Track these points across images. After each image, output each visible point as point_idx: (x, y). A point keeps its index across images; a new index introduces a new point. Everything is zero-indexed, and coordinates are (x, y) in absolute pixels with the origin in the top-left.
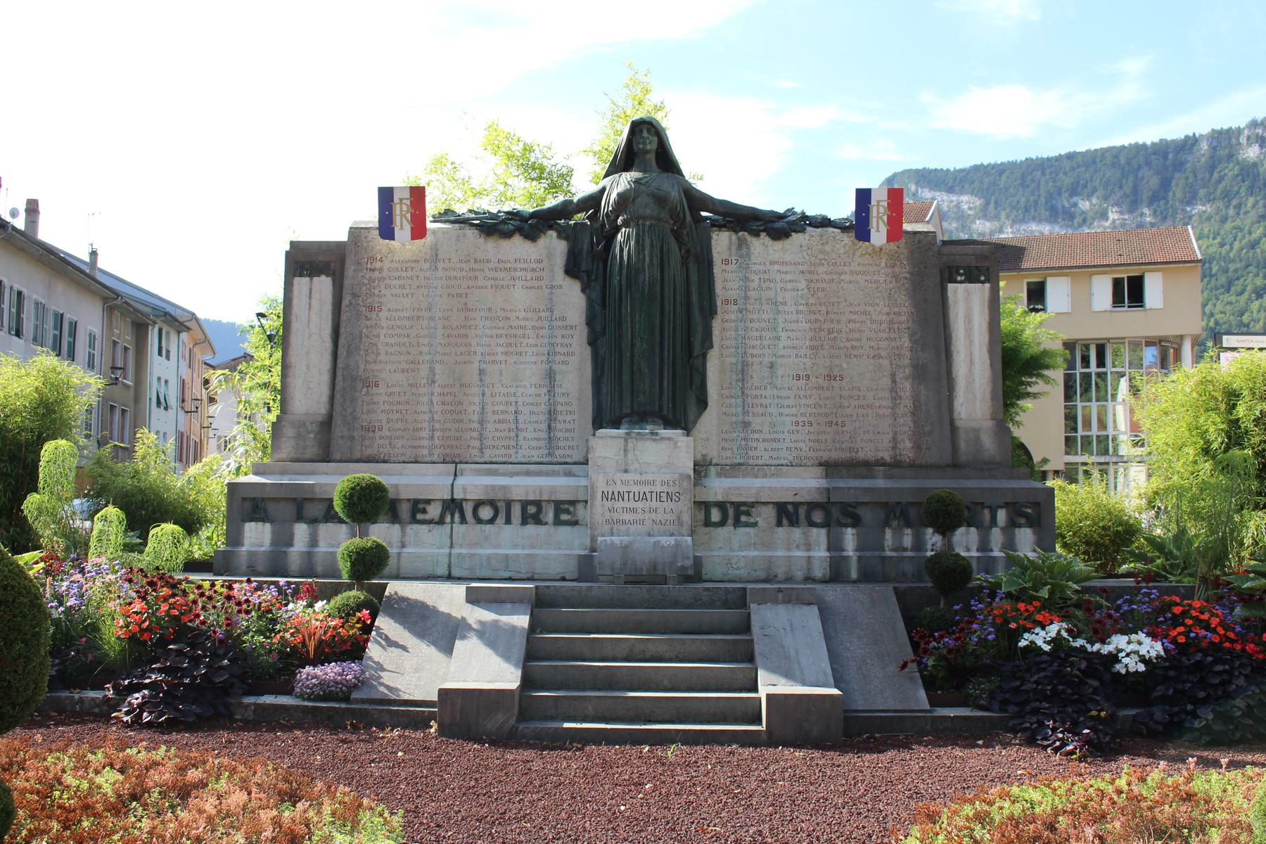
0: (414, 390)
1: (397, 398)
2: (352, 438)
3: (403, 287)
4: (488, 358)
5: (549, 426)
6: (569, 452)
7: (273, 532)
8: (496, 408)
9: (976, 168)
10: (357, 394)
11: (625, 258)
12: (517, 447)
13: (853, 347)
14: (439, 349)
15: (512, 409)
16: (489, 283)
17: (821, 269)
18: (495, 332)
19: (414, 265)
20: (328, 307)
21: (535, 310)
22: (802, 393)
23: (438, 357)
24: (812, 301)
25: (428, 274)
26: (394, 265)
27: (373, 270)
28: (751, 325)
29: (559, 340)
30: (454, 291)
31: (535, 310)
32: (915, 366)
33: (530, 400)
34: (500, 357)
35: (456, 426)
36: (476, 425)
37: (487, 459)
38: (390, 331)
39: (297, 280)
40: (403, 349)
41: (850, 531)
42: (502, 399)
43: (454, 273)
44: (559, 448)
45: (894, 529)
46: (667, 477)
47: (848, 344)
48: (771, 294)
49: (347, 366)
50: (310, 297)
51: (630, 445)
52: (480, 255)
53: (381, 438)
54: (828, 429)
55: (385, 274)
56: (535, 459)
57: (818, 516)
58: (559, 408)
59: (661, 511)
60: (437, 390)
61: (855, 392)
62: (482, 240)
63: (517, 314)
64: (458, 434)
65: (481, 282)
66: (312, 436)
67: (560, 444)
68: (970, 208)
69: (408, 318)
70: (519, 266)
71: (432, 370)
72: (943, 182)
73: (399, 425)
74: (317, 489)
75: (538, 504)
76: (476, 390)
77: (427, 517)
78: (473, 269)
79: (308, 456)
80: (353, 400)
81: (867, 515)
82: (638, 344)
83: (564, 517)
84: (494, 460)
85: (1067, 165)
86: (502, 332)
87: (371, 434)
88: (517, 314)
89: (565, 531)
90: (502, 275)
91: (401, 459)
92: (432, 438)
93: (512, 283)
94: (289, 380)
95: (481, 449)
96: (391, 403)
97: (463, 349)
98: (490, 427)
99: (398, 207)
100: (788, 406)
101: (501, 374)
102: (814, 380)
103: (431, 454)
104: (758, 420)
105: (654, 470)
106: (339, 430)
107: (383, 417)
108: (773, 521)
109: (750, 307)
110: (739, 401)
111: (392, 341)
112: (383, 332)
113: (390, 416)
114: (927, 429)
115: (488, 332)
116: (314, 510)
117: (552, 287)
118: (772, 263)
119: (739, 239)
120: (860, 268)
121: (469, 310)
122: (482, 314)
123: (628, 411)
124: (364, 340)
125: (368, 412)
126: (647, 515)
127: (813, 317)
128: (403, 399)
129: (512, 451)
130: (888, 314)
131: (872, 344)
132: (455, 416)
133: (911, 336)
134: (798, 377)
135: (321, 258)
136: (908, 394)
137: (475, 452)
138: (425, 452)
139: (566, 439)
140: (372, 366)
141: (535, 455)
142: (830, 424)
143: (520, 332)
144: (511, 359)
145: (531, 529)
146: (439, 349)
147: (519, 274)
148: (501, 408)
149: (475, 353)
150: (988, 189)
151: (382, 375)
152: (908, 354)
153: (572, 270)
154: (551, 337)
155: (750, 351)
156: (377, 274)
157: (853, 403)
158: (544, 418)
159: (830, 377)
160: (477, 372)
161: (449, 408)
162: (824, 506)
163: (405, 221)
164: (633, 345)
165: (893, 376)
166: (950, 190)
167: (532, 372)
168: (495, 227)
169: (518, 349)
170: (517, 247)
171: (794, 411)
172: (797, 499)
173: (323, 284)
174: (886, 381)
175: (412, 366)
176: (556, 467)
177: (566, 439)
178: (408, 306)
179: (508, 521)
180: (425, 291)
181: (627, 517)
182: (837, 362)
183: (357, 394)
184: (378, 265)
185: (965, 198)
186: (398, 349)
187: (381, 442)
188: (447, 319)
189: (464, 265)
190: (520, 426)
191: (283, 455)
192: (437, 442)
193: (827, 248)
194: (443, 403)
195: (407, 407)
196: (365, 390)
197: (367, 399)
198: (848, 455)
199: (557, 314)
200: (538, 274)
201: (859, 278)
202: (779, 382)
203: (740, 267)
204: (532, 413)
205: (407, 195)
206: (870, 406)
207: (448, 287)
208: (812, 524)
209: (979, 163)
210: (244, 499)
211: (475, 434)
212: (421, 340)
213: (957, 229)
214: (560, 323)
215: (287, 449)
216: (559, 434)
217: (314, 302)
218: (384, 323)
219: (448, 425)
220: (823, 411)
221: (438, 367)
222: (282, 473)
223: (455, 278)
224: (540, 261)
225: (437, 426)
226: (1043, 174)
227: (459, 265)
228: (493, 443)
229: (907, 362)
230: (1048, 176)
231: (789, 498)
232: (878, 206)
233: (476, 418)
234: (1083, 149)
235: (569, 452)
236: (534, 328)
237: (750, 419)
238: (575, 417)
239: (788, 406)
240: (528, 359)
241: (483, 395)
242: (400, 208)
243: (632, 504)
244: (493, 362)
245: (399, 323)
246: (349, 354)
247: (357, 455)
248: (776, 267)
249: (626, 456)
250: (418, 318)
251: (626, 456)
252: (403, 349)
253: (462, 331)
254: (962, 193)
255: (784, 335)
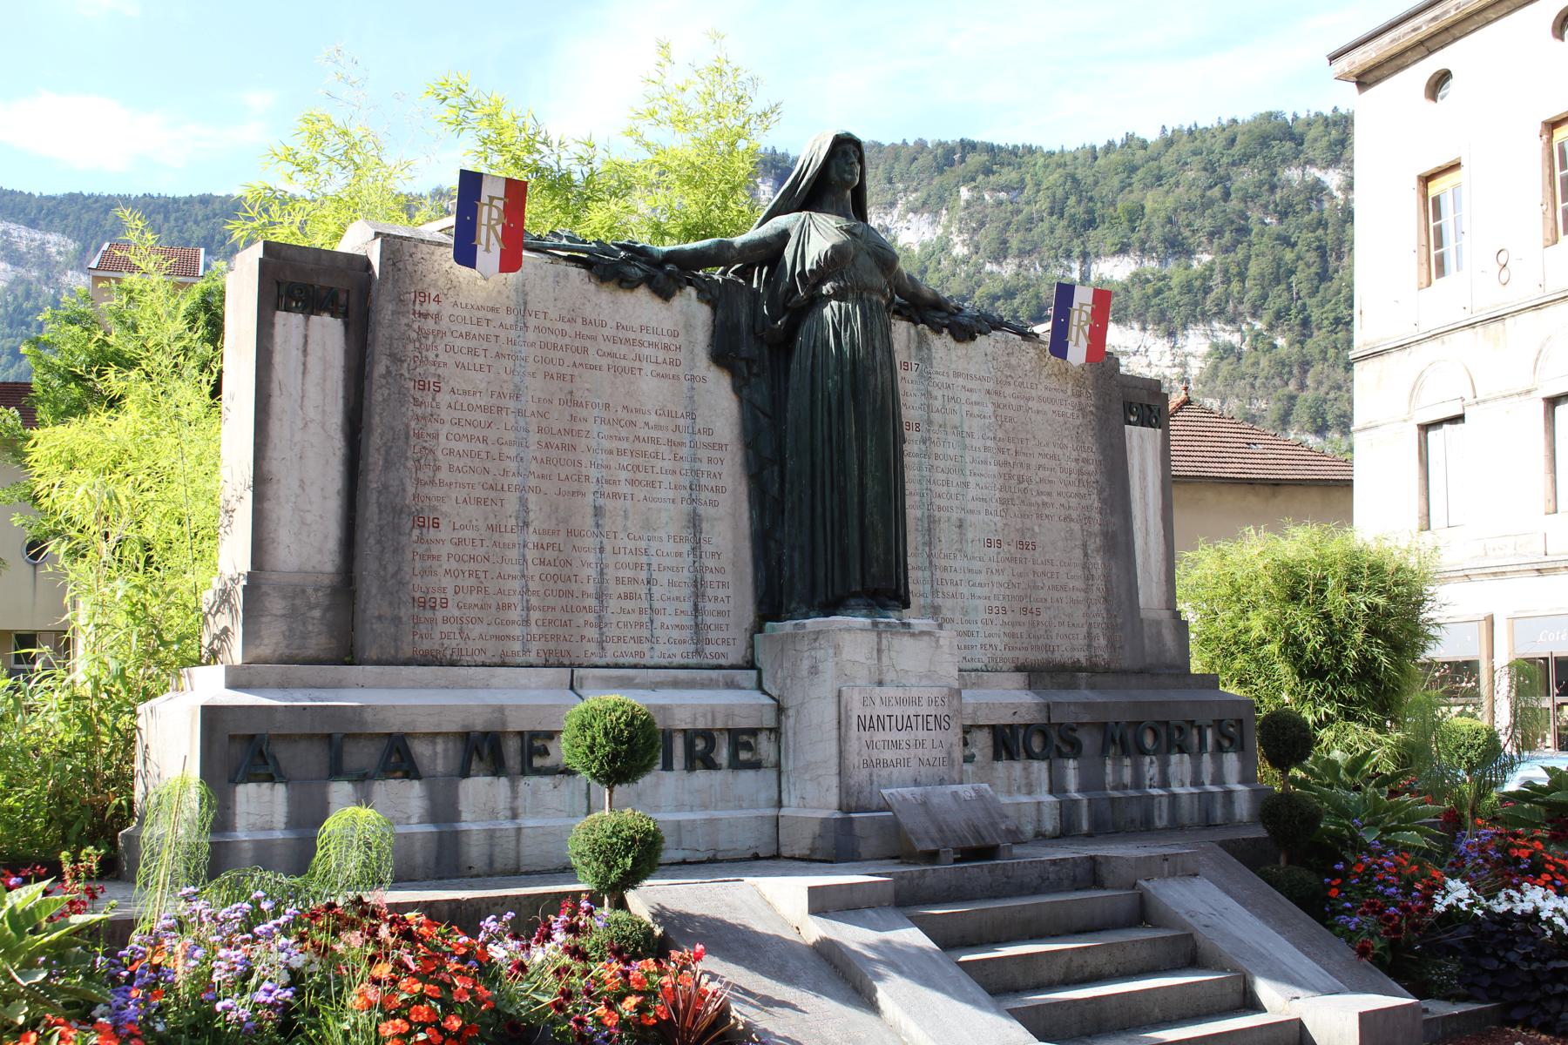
0: (496, 536)
1: (469, 550)
2: (397, 620)
3: (472, 352)
4: (607, 489)
5: (696, 605)
6: (722, 649)
7: (292, 801)
8: (621, 574)
9: (72, 198)
10: (404, 539)
11: (847, 349)
12: (652, 639)
13: (1044, 504)
14: (534, 467)
15: (643, 575)
16: (604, 362)
17: (1008, 390)
18: (616, 444)
19: (490, 316)
20: (337, 375)
21: (670, 414)
22: (994, 566)
23: (533, 482)
24: (1000, 435)
25: (513, 334)
26: (458, 312)
27: (425, 316)
28: (936, 463)
29: (704, 467)
30: (553, 370)
31: (670, 414)
32: (1105, 534)
33: (668, 562)
34: (624, 488)
35: (563, 602)
36: (591, 602)
37: (609, 659)
38: (456, 430)
39: (280, 316)
40: (477, 463)
41: (1071, 764)
42: (629, 559)
43: (552, 339)
44: (709, 642)
45: (1114, 759)
46: (935, 693)
47: (1039, 499)
48: (955, 419)
49: (386, 487)
50: (305, 352)
51: (884, 642)
52: (589, 312)
53: (446, 620)
54: (1023, 619)
55: (444, 324)
56: (678, 660)
57: (1036, 744)
58: (708, 577)
59: (928, 744)
60: (533, 538)
61: (1048, 568)
62: (592, 287)
63: (647, 418)
64: (566, 617)
65: (593, 359)
66: (317, 613)
67: (712, 635)
68: (60, 253)
69: (484, 409)
70: (647, 338)
71: (523, 503)
72: (23, 210)
73: (473, 599)
74: (369, 717)
75: (708, 735)
76: (590, 542)
77: (548, 762)
78: (579, 335)
79: (310, 652)
80: (398, 550)
81: (1088, 740)
82: (870, 484)
83: (744, 755)
84: (621, 661)
85: (200, 212)
86: (625, 445)
87: (429, 614)
88: (647, 418)
89: (747, 776)
90: (623, 349)
91: (479, 659)
92: (526, 622)
93: (637, 364)
94: (267, 505)
95: (601, 644)
96: (460, 559)
97: (570, 470)
98: (613, 604)
99: (486, 209)
100: (980, 585)
101: (626, 517)
102: (1005, 547)
103: (526, 651)
104: (949, 603)
105: (913, 681)
106: (373, 603)
107: (447, 582)
108: (989, 752)
109: (934, 437)
110: (927, 574)
111: (461, 446)
112: (444, 430)
113: (460, 582)
114: (1119, 621)
115: (606, 444)
116: (360, 756)
117: (693, 378)
118: (957, 375)
119: (918, 334)
120: (1047, 394)
121: (577, 404)
122: (596, 412)
123: (859, 589)
124: (413, 441)
125: (424, 573)
126: (913, 751)
127: (1002, 458)
128: (481, 551)
129: (645, 646)
130: (1077, 460)
131: (1063, 501)
132: (560, 585)
133: (1100, 492)
134: (989, 543)
135: (323, 281)
136: (1100, 572)
137: (592, 647)
138: (517, 646)
139: (719, 627)
140: (427, 490)
141: (679, 653)
142: (1025, 610)
143: (651, 448)
144: (640, 492)
145: (701, 777)
146: (534, 467)
147: (647, 351)
148: (629, 573)
149: (587, 478)
150: (87, 230)
151: (445, 508)
152: (1097, 516)
153: (722, 354)
154: (694, 459)
155: (937, 502)
156: (430, 324)
157: (1048, 583)
158: (687, 591)
159: (1022, 545)
160: (590, 511)
161: (551, 570)
162: (1043, 730)
163: (493, 239)
164: (862, 485)
165: (1085, 546)
166: (32, 224)
167: (669, 515)
168: (617, 267)
169: (650, 477)
170: (640, 306)
171: (985, 591)
172: (1017, 720)
173: (328, 331)
174: (1078, 553)
175: (492, 494)
176: (714, 674)
177: (719, 627)
178: (483, 386)
179: (668, 766)
180: (509, 364)
181: (889, 755)
182: (1028, 523)
183: (404, 539)
184: (432, 307)
185: (53, 238)
186: (468, 461)
187: (446, 628)
188: (543, 415)
189: (566, 326)
190: (657, 605)
191: (265, 650)
192: (534, 630)
193: (1013, 361)
194: (542, 562)
195: (486, 566)
196: (416, 532)
197: (421, 549)
198: (1044, 656)
199: (700, 424)
200: (672, 355)
201: (1047, 407)
202: (969, 549)
203: (921, 375)
204: (671, 583)
205: (500, 191)
206: (1064, 588)
207: (544, 360)
208: (1031, 756)
209: (76, 191)
210: (232, 738)
211: (591, 617)
212: (505, 449)
213: (39, 280)
214: (705, 439)
215: (273, 639)
216: (709, 620)
217: (313, 360)
218: (445, 413)
219: (551, 601)
220: (1016, 592)
221: (532, 498)
222: (283, 685)
223: (555, 347)
224: (675, 334)
225: (534, 601)
226: (166, 219)
227: (560, 326)
228: (617, 632)
229: (1096, 528)
230: (172, 223)
231: (1007, 719)
232: (1081, 310)
233: (591, 588)
234: (223, 194)
235: (722, 649)
236: (671, 443)
237: (939, 601)
238: (730, 592)
239: (980, 585)
240: (663, 493)
241: (602, 550)
242: (487, 211)
243: (894, 736)
244: (615, 496)
245: (470, 416)
246: (388, 464)
247: (407, 652)
248: (961, 381)
249: (879, 659)
250: (500, 410)
251: (879, 659)
252: (477, 463)
253: (567, 440)
254: (49, 228)
255: (971, 480)
